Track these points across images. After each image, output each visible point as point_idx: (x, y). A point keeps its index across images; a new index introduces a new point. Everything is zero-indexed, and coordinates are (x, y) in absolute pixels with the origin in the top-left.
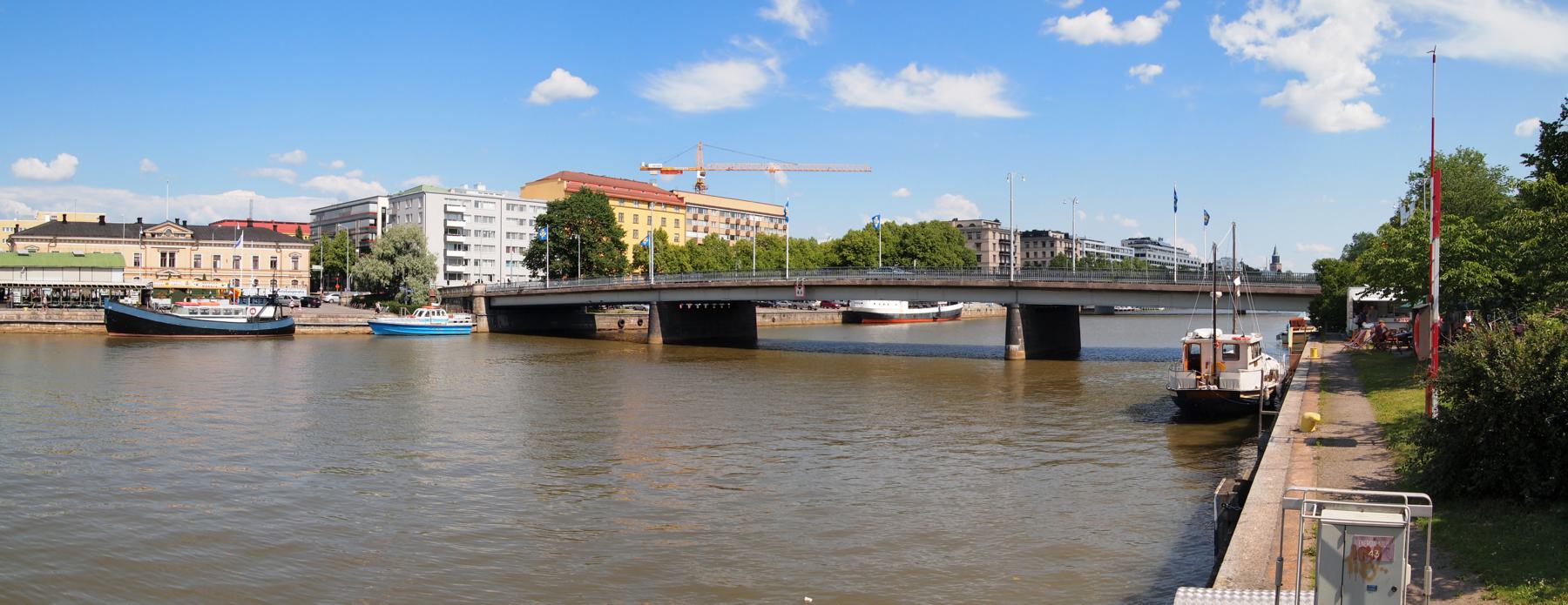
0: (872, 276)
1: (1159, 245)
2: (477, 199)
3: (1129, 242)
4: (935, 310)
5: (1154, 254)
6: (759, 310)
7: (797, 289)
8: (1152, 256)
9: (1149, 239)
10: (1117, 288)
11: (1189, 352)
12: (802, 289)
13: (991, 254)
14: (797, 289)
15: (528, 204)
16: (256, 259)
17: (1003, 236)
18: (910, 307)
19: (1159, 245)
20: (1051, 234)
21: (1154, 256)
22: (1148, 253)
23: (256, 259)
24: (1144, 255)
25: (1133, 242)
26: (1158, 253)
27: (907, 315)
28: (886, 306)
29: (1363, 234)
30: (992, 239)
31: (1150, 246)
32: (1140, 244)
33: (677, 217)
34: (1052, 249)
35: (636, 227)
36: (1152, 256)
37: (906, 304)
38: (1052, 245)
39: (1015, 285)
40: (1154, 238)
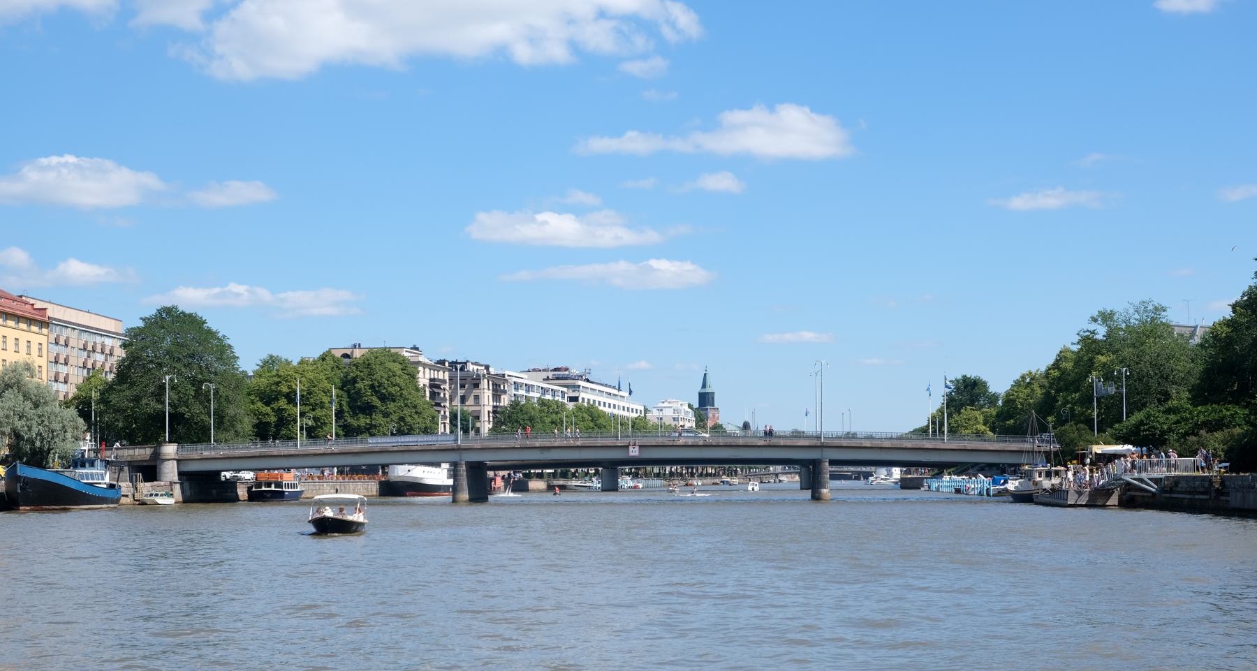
7: (631, 448)
12: (637, 448)
33: (17, 334)
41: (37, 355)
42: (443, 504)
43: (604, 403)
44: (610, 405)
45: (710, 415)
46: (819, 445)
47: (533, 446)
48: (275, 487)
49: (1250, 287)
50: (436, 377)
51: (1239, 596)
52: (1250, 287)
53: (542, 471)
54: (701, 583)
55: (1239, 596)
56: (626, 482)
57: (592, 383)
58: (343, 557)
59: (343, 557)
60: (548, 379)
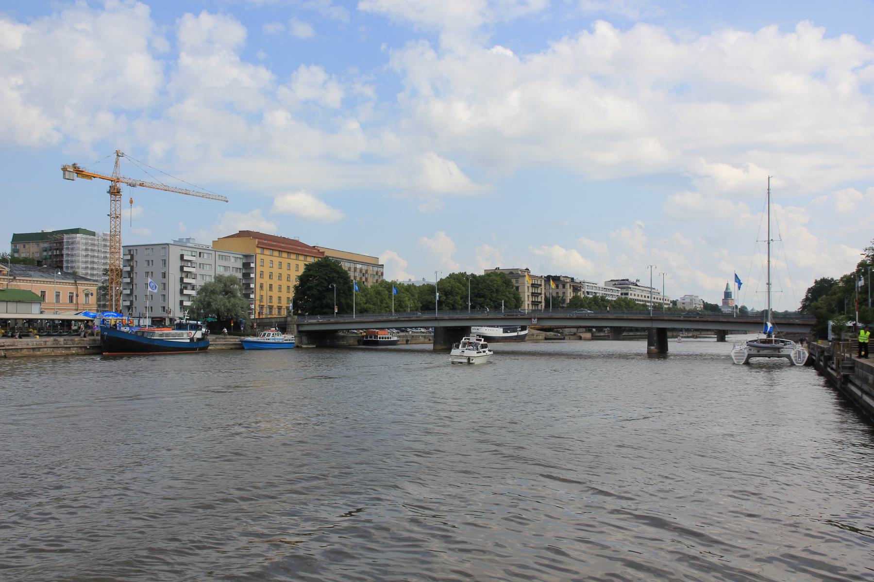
0: (112, 314)
1: (637, 285)
2: (201, 251)
3: (614, 283)
4: (515, 334)
5: (635, 293)
6: (472, 327)
7: (533, 320)
8: (633, 295)
9: (628, 280)
10: (705, 320)
11: (748, 360)
12: (536, 320)
13: (526, 294)
14: (533, 320)
15: (231, 255)
16: (58, 296)
17: (533, 281)
18: (503, 333)
19: (637, 285)
20: (562, 279)
21: (635, 295)
22: (630, 292)
23: (58, 296)
24: (627, 294)
25: (616, 283)
26: (637, 292)
27: (502, 337)
28: (492, 332)
29: (845, 276)
30: (528, 281)
31: (630, 286)
32: (623, 284)
33: (298, 262)
34: (564, 290)
35: (280, 271)
36: (633, 295)
37: (501, 330)
38: (564, 287)
39: (653, 318)
40: (633, 280)
41: (278, 268)
42: (313, 348)
43: (533, 294)
44: (642, 296)
45: (730, 302)
46: (649, 318)
47: (622, 318)
48: (374, 338)
49: (465, 273)
50: (536, 283)
51: (125, 389)
52: (465, 273)
53: (197, 322)
54: (512, 457)
55: (125, 389)
56: (674, 346)
57: (639, 286)
58: (181, 406)
59: (181, 406)
60: (615, 284)
